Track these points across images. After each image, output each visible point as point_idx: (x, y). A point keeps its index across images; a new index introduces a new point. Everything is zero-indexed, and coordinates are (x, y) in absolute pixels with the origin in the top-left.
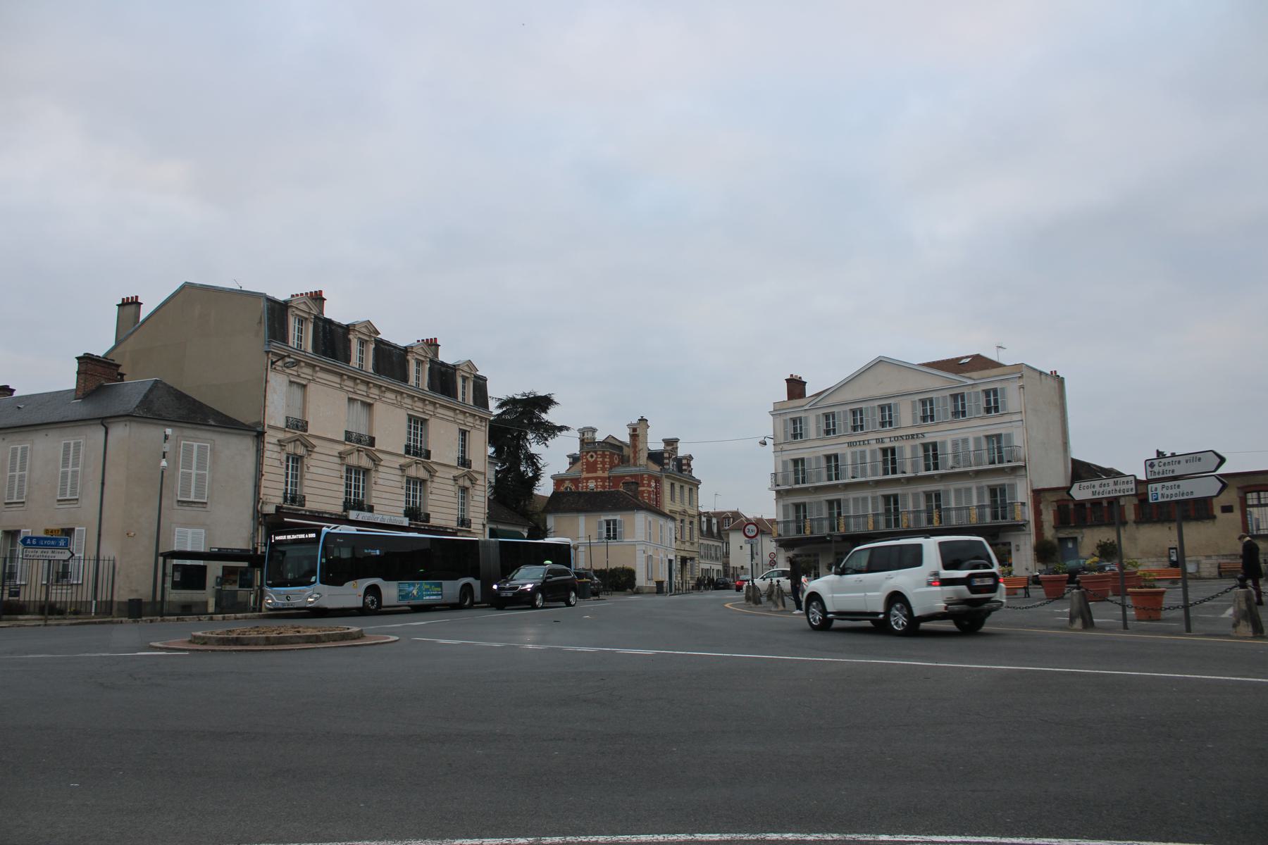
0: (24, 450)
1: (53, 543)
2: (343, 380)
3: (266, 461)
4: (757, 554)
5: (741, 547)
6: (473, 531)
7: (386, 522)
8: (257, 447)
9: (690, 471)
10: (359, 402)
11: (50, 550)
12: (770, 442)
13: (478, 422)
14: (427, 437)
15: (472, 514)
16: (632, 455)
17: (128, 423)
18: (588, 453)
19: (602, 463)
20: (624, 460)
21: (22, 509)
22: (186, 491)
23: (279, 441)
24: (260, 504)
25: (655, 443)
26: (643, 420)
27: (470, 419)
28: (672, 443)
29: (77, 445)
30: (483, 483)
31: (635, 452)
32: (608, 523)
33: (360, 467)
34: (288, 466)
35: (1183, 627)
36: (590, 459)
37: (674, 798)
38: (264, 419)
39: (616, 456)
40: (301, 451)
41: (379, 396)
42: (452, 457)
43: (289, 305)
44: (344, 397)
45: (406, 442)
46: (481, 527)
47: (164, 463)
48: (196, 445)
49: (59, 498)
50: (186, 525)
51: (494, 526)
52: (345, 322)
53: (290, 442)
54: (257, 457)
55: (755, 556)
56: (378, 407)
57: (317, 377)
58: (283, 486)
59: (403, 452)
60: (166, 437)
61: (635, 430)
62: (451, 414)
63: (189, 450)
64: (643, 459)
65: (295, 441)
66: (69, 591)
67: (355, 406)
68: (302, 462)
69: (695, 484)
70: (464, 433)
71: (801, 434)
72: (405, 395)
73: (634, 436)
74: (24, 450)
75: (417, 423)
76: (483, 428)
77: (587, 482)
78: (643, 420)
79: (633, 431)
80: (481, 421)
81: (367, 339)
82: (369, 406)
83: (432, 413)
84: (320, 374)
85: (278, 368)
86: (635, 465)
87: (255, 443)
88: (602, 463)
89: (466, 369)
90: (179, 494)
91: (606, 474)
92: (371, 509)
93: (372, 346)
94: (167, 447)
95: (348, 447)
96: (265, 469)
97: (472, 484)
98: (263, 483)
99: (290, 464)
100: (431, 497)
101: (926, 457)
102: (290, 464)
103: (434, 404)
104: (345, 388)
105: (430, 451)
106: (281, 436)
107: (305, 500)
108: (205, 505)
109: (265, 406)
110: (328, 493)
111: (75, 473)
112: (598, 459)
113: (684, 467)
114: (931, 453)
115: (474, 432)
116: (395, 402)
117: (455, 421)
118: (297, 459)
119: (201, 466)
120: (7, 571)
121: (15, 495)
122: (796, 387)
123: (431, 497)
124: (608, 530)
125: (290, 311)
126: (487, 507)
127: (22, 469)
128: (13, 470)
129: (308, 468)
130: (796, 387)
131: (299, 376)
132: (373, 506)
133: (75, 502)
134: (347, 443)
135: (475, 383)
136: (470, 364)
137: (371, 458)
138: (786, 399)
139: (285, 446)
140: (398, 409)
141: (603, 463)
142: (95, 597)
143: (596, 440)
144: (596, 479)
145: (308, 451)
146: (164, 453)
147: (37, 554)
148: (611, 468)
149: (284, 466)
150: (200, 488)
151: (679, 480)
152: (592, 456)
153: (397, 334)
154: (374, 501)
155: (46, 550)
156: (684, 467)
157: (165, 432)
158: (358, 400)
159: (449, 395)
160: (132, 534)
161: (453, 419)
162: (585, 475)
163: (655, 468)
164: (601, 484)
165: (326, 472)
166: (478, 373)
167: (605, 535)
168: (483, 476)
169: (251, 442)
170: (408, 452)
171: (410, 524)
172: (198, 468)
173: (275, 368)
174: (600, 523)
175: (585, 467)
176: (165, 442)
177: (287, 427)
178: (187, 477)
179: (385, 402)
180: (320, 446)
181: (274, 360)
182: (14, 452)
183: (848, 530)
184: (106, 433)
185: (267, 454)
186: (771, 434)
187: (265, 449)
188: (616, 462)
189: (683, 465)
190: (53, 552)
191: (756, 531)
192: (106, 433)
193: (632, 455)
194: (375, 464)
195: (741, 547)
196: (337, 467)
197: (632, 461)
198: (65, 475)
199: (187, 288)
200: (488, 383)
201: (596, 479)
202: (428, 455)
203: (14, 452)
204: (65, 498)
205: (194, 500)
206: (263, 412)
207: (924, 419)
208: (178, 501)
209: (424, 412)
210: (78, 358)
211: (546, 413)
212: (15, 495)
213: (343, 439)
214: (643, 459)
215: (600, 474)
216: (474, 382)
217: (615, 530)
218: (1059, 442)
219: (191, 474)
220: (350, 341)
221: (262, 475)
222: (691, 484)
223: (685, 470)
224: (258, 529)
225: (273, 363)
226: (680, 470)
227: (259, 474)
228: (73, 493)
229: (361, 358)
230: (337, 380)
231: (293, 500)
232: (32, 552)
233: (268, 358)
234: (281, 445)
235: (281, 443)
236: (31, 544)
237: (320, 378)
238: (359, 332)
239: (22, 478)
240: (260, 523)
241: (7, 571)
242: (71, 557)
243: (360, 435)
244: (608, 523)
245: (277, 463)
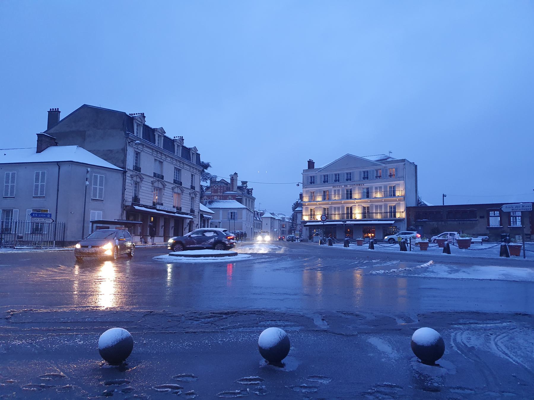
0: (13, 174)
1: (45, 215)
2: (143, 147)
3: (127, 184)
4: (272, 227)
5: (267, 224)
6: (195, 215)
7: (169, 210)
8: (123, 177)
9: (252, 194)
10: (158, 161)
11: (43, 219)
12: (301, 185)
13: (197, 172)
14: (181, 176)
16: (231, 187)
17: (71, 165)
19: (220, 189)
20: (228, 189)
21: (13, 200)
22: (95, 195)
23: (131, 175)
24: (124, 202)
25: (239, 184)
26: (236, 174)
27: (195, 170)
28: (244, 183)
29: (43, 174)
30: (199, 196)
31: (232, 186)
32: (232, 213)
33: (159, 188)
35: (481, 244)
36: (215, 188)
37: (187, 336)
38: (126, 166)
40: (138, 180)
41: (165, 159)
43: (134, 118)
44: (153, 158)
45: (173, 179)
46: (198, 213)
47: (87, 183)
48: (99, 175)
49: (34, 196)
50: (94, 209)
52: (153, 127)
53: (135, 176)
54: (123, 182)
55: (272, 227)
56: (165, 163)
57: (144, 150)
60: (88, 172)
62: (189, 168)
63: (96, 177)
65: (136, 176)
66: (36, 237)
67: (157, 162)
68: (139, 185)
69: (254, 199)
70: (192, 175)
71: (314, 182)
72: (174, 159)
73: (232, 179)
74: (13, 174)
75: (178, 171)
76: (199, 174)
77: (214, 197)
78: (236, 174)
79: (232, 178)
80: (198, 171)
81: (161, 135)
82: (161, 163)
83: (182, 167)
84: (145, 149)
85: (131, 145)
87: (123, 176)
88: (220, 189)
89: (194, 150)
90: (4, 195)
91: (221, 194)
92: (162, 204)
94: (88, 176)
96: (126, 187)
97: (195, 196)
98: (126, 193)
101: (347, 194)
103: (183, 163)
104: (154, 155)
106: (131, 173)
107: (140, 201)
108: (102, 201)
109: (126, 160)
110: (147, 198)
111: (42, 186)
112: (219, 188)
113: (250, 193)
114: (349, 193)
115: (196, 175)
116: (170, 162)
119: (101, 185)
120: (4, 227)
121: (39, 193)
122: (311, 164)
124: (232, 216)
125: (134, 121)
127: (13, 182)
128: (7, 182)
129: (141, 187)
130: (311, 164)
131: (138, 149)
132: (163, 204)
133: (13, 198)
134: (154, 177)
138: (307, 169)
139: (133, 178)
140: (171, 165)
141: (221, 189)
142: (55, 240)
143: (217, 181)
144: (217, 196)
145: (141, 180)
146: (87, 178)
147: (38, 220)
148: (223, 192)
150: (12, 192)
151: (248, 197)
152: (216, 187)
153: (170, 134)
154: (163, 202)
155: (42, 219)
156: (250, 193)
157: (87, 170)
158: (158, 160)
160: (73, 212)
161: (189, 170)
162: (213, 194)
163: (240, 192)
164: (219, 198)
165: (147, 189)
166: (197, 152)
167: (230, 217)
169: (121, 175)
171: (177, 211)
172: (100, 186)
173: (129, 145)
175: (213, 191)
176: (87, 174)
177: (134, 170)
178: (95, 189)
179: (166, 161)
181: (129, 141)
182: (8, 175)
183: (396, 217)
184: (59, 168)
185: (127, 181)
186: (302, 181)
187: (126, 178)
188: (225, 189)
189: (249, 192)
190: (44, 220)
191: (326, 218)
192: (59, 168)
193: (231, 187)
194: (163, 187)
195: (267, 224)
196: (151, 187)
197: (231, 190)
198: (37, 186)
199: (85, 106)
202: (162, 177)
203: (8, 175)
204: (38, 196)
205: (98, 199)
206: (125, 163)
207: (364, 178)
208: (92, 199)
209: (180, 167)
210: (308, 161)
211: (206, 169)
212: (39, 193)
213: (153, 176)
214: (235, 188)
215: (219, 194)
216: (196, 155)
217: (234, 216)
218: (415, 189)
219: (38, 184)
220: (155, 135)
221: (125, 189)
222: (252, 199)
223: (250, 194)
224: (123, 212)
225: (129, 143)
226: (249, 194)
227: (124, 189)
228: (100, 196)
229: (159, 143)
230: (151, 151)
232: (35, 219)
233: (127, 140)
234: (132, 177)
235: (132, 176)
236: (35, 216)
237: (145, 150)
238: (158, 132)
239: (12, 187)
240: (124, 209)
241: (4, 227)
242: (53, 222)
243: (159, 175)
244: (232, 213)
245: (130, 185)
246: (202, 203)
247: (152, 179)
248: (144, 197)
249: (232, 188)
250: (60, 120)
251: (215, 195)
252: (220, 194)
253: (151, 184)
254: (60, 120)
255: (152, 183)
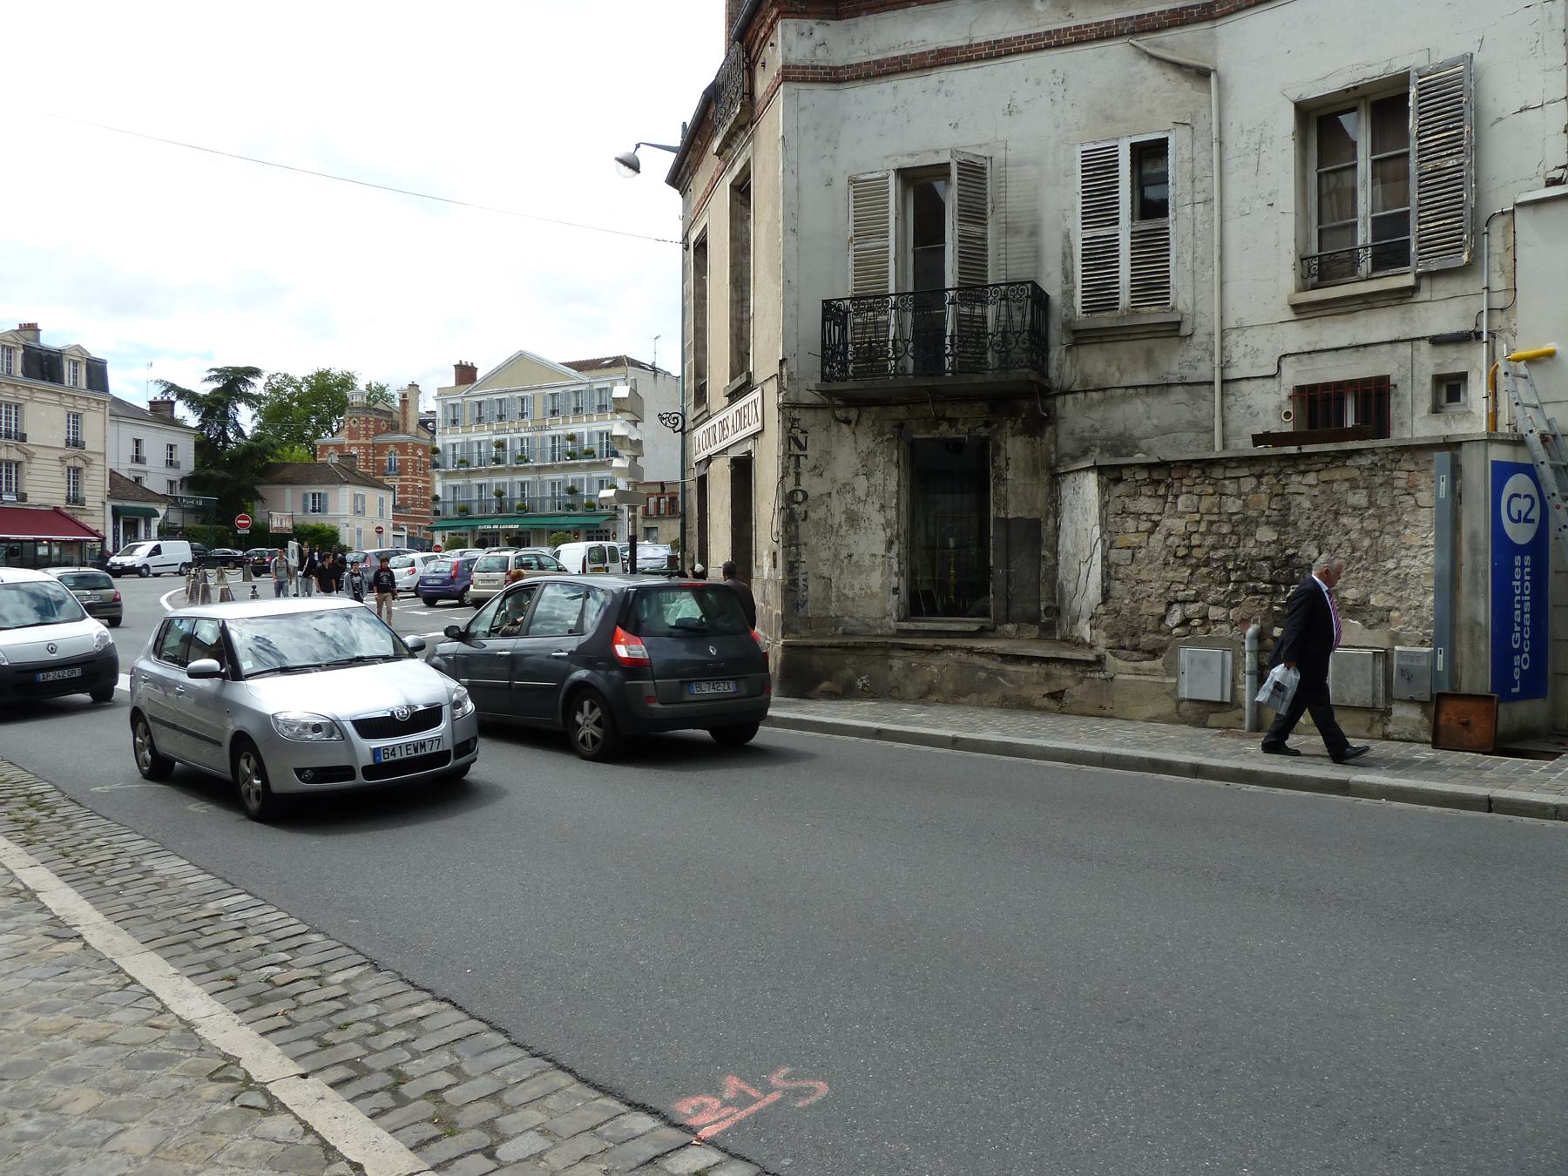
2: (32, 392)
15: (86, 493)
16: (401, 422)
18: (350, 418)
19: (366, 429)
20: (394, 428)
31: (405, 419)
34: (69, 476)
36: (352, 425)
39: (383, 422)
40: (79, 464)
42: (58, 437)
45: (65, 437)
46: (101, 505)
51: (118, 503)
58: (65, 491)
59: (63, 445)
61: (404, 396)
64: (412, 426)
75: (75, 419)
86: (405, 432)
88: (366, 429)
91: (370, 441)
93: (21, 352)
95: (68, 453)
99: (72, 474)
100: (28, 477)
102: (72, 474)
105: (25, 435)
117: (61, 405)
118: (77, 470)
123: (28, 477)
124: (314, 502)
126: (108, 481)
135: (88, 365)
136: (78, 348)
137: (22, 452)
141: (367, 429)
144: (359, 446)
149: (66, 476)
159: (52, 380)
168: (102, 457)
170: (68, 443)
174: (305, 497)
180: (39, 453)
197: (401, 428)
200: (109, 367)
201: (359, 446)
202: (23, 438)
214: (412, 426)
215: (362, 440)
231: (75, 502)
246: (895, 693)
247: (62, 454)
248: (56, 479)
249: (405, 425)
250: (1307, 710)
251: (354, 445)
252: (367, 442)
253: (59, 463)
254: (1307, 710)
255: (62, 460)
